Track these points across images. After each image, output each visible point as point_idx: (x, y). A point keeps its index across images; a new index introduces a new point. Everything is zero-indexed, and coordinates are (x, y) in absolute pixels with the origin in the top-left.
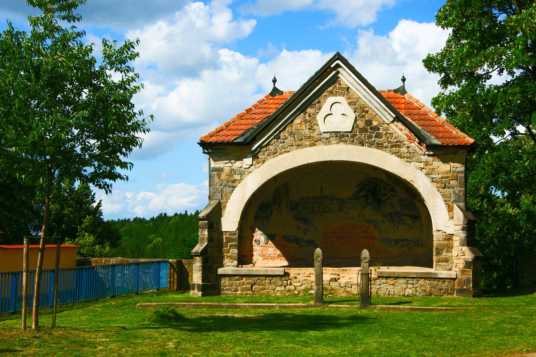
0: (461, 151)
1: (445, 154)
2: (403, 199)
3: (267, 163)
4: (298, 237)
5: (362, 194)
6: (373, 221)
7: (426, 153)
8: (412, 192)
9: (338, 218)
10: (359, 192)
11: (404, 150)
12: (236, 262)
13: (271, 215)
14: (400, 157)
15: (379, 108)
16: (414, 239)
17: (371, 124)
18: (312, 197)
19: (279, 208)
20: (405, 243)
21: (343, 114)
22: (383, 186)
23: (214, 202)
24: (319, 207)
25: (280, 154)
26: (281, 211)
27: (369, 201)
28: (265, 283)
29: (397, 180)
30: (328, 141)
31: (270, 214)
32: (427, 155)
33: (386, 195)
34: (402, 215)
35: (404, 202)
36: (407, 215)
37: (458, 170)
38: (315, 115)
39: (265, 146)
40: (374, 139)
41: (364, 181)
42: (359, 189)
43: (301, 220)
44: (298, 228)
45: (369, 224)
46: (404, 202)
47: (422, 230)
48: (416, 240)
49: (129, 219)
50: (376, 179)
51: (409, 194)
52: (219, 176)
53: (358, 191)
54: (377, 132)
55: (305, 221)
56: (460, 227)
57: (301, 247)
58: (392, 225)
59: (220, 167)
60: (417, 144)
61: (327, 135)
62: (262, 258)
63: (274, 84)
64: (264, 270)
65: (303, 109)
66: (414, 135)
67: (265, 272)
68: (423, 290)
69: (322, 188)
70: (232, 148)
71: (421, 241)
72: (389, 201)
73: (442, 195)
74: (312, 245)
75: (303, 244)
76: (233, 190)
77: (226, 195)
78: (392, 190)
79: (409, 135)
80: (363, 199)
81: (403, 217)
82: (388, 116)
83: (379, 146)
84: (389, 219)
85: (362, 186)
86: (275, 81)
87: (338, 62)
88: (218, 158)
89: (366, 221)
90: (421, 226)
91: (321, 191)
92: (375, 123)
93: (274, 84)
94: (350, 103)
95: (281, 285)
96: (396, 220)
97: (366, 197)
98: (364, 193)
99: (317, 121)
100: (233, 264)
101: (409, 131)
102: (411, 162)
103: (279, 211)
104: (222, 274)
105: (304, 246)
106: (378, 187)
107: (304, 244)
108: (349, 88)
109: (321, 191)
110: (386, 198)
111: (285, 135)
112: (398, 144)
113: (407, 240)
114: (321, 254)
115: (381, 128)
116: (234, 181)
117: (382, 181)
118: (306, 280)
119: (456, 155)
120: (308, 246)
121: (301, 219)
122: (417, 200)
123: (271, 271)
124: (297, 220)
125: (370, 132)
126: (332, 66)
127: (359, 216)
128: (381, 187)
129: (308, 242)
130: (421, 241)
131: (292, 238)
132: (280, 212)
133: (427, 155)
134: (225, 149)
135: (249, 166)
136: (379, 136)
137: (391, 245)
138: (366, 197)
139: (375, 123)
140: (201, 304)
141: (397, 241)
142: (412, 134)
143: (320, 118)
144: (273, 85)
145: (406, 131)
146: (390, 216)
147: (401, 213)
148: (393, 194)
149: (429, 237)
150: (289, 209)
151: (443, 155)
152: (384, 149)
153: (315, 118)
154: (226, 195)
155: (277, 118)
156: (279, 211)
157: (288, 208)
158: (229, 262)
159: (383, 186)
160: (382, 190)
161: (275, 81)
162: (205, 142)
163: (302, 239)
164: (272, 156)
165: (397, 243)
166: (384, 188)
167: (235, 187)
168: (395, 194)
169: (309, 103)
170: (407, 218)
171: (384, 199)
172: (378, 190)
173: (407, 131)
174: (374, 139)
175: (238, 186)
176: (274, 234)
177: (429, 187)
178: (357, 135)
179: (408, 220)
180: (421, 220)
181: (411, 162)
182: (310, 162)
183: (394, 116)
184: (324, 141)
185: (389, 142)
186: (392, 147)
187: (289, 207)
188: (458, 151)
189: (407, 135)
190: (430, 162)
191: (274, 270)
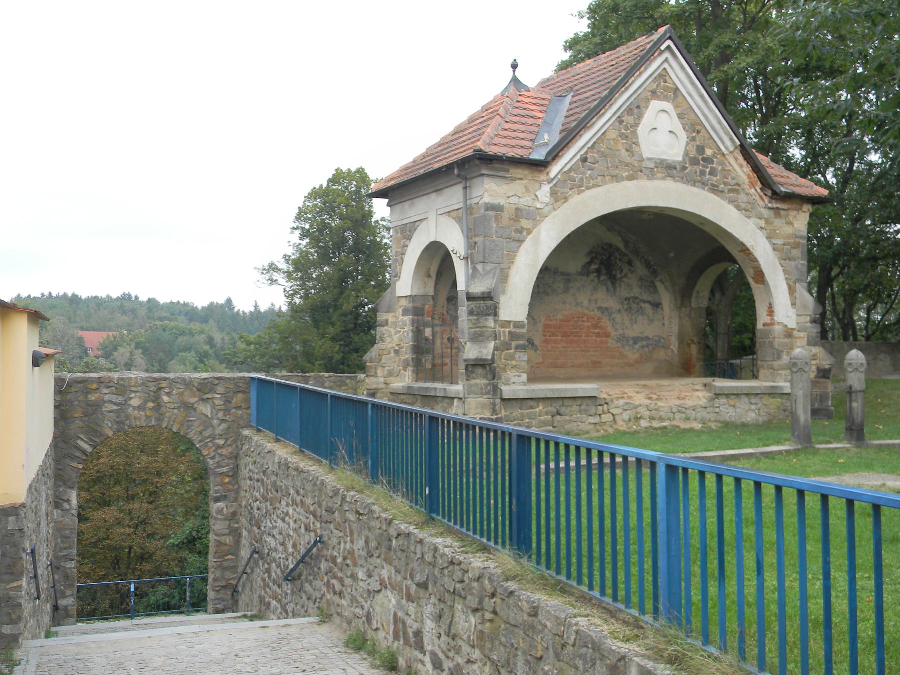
5: (594, 267)
6: (607, 309)
9: (564, 303)
10: (590, 263)
11: (742, 198)
12: (525, 377)
14: (738, 208)
15: (718, 127)
17: (704, 153)
20: (645, 343)
21: (670, 132)
22: (619, 257)
25: (588, 188)
27: (603, 278)
28: (571, 411)
30: (651, 175)
40: (708, 177)
47: (664, 325)
48: (657, 339)
49: (179, 302)
50: (611, 246)
52: (498, 219)
56: (808, 319)
63: (514, 71)
68: (767, 413)
71: (662, 340)
73: (784, 271)
76: (520, 246)
77: (509, 255)
80: (595, 275)
82: (728, 143)
83: (714, 189)
84: (626, 307)
86: (515, 66)
90: (663, 319)
92: (709, 152)
93: (514, 71)
95: (596, 414)
99: (637, 138)
106: (612, 258)
108: (677, 88)
112: (736, 189)
113: (647, 338)
115: (715, 160)
116: (520, 231)
117: (618, 249)
125: (703, 166)
130: (662, 340)
136: (713, 173)
138: (598, 271)
139: (709, 152)
141: (636, 340)
144: (512, 72)
145: (748, 170)
152: (719, 194)
153: (635, 133)
154: (509, 255)
158: (515, 376)
159: (619, 257)
160: (618, 262)
161: (515, 66)
165: (635, 343)
166: (620, 260)
167: (523, 242)
174: (708, 177)
175: (527, 241)
179: (648, 308)
180: (662, 309)
183: (739, 143)
185: (725, 184)
186: (730, 191)
189: (749, 177)
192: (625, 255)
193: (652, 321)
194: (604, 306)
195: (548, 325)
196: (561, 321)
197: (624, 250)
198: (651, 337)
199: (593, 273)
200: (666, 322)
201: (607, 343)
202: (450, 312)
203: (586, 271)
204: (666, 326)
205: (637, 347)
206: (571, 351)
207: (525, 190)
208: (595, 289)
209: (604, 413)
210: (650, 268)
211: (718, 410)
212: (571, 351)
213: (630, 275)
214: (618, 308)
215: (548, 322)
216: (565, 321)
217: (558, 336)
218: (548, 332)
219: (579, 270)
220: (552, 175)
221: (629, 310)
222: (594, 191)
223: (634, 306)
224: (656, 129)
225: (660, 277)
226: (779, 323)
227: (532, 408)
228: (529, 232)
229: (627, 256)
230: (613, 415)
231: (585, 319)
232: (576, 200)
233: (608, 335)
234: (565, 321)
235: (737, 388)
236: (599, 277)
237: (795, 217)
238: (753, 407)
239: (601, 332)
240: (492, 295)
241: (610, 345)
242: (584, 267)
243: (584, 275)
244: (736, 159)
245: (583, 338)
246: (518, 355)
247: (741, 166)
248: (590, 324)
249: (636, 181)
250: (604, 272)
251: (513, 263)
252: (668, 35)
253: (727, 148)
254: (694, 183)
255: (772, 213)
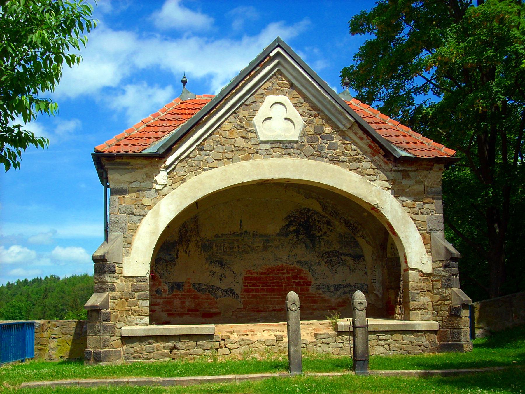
0: (436, 167)
1: (417, 170)
2: (342, 234)
3: (189, 182)
4: (212, 286)
5: (292, 228)
6: (306, 262)
7: (394, 168)
8: (352, 226)
10: (288, 226)
12: (147, 319)
13: (177, 257)
14: (361, 174)
16: (357, 285)
18: (229, 233)
19: (186, 249)
23: (115, 236)
24: (238, 247)
26: (189, 252)
27: (301, 237)
29: (335, 211)
30: (268, 154)
31: (176, 256)
32: (395, 171)
33: (321, 230)
34: (341, 254)
35: (343, 239)
36: (347, 255)
37: (434, 190)
38: (250, 119)
39: (183, 160)
40: (326, 151)
41: (294, 212)
42: (287, 223)
43: (216, 264)
44: (213, 274)
45: (302, 266)
46: (343, 239)
47: (366, 273)
50: (309, 210)
51: (349, 229)
53: (287, 225)
54: (330, 142)
55: (221, 264)
57: (217, 298)
58: (330, 267)
59: (122, 188)
60: (382, 157)
61: (268, 146)
62: (166, 314)
64: (188, 328)
65: (233, 111)
66: (378, 146)
67: (189, 330)
69: (241, 222)
70: (139, 162)
71: (365, 287)
72: (325, 237)
74: (231, 295)
75: (220, 293)
78: (329, 223)
79: (372, 144)
81: (343, 257)
84: (326, 260)
85: (292, 219)
87: (278, 49)
88: (120, 176)
89: (298, 262)
90: (366, 268)
91: (241, 226)
94: (294, 104)
96: (334, 260)
97: (297, 232)
98: (295, 228)
100: (143, 321)
101: (371, 140)
102: (375, 180)
103: (188, 252)
104: (128, 336)
105: (221, 297)
106: (311, 220)
107: (221, 294)
109: (241, 226)
110: (321, 233)
111: (210, 145)
114: (298, 299)
117: (316, 212)
118: (243, 340)
119: (432, 172)
120: (225, 296)
121: (216, 261)
122: (359, 235)
123: (197, 329)
124: (211, 263)
126: (272, 55)
127: (288, 257)
128: (315, 220)
129: (226, 292)
131: (205, 287)
132: (188, 254)
133: (395, 171)
134: (128, 164)
135: (163, 186)
137: (330, 292)
138: (297, 232)
140: (121, 382)
142: (376, 144)
143: (257, 120)
145: (368, 141)
146: (327, 256)
147: (340, 251)
148: (329, 229)
149: (375, 281)
150: (200, 249)
151: (414, 171)
155: (200, 122)
156: (188, 252)
157: (198, 247)
159: (317, 219)
160: (317, 223)
162: (103, 152)
163: (217, 288)
164: (193, 172)
165: (337, 290)
166: (319, 221)
167: (144, 215)
168: (332, 228)
169: (242, 103)
170: (348, 258)
171: (319, 234)
172: (312, 224)
173: (369, 141)
175: (148, 214)
176: (181, 283)
177: (399, 213)
178: (305, 145)
179: (350, 261)
180: (364, 260)
181: (375, 180)
182: (245, 180)
184: (264, 152)
186: (350, 161)
187: (200, 246)
188: (433, 166)
189: (370, 146)
190: (399, 180)
191: (201, 328)
192: (323, 216)
193: (354, 270)
194: (303, 260)
195: (249, 277)
196: (261, 273)
197: (323, 213)
198: (352, 284)
199: (292, 233)
200: (368, 271)
201: (308, 290)
202: (158, 271)
203: (284, 232)
204: (369, 274)
205: (338, 293)
206: (271, 298)
207: (145, 176)
208: (294, 246)
209: (221, 347)
210: (350, 226)
211: (341, 345)
212: (271, 298)
213: (329, 233)
214: (318, 261)
215: (248, 275)
216: (265, 273)
217: (259, 286)
218: (248, 283)
219: (278, 231)
220: (168, 163)
221: (329, 262)
222: (210, 172)
223: (334, 259)
224: (270, 118)
225: (361, 233)
226: (413, 269)
227: (150, 343)
228: (150, 207)
229: (325, 217)
230: (229, 349)
231: (285, 271)
232: (192, 180)
233: (309, 284)
234: (265, 273)
235: (389, 325)
236: (297, 236)
237: (426, 176)
238: (382, 343)
239: (302, 281)
240: (106, 257)
241: (310, 292)
242: (282, 229)
243: (282, 235)
244: (356, 134)
245: (284, 287)
246: (140, 303)
247: (361, 139)
248: (290, 275)
249: (252, 160)
250: (302, 232)
251: (136, 232)
252: (277, 44)
253: (344, 126)
254: (313, 156)
255: (399, 175)
